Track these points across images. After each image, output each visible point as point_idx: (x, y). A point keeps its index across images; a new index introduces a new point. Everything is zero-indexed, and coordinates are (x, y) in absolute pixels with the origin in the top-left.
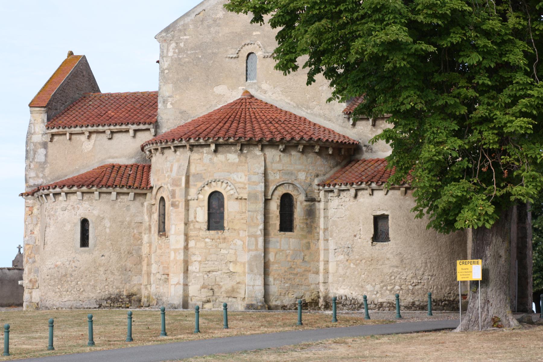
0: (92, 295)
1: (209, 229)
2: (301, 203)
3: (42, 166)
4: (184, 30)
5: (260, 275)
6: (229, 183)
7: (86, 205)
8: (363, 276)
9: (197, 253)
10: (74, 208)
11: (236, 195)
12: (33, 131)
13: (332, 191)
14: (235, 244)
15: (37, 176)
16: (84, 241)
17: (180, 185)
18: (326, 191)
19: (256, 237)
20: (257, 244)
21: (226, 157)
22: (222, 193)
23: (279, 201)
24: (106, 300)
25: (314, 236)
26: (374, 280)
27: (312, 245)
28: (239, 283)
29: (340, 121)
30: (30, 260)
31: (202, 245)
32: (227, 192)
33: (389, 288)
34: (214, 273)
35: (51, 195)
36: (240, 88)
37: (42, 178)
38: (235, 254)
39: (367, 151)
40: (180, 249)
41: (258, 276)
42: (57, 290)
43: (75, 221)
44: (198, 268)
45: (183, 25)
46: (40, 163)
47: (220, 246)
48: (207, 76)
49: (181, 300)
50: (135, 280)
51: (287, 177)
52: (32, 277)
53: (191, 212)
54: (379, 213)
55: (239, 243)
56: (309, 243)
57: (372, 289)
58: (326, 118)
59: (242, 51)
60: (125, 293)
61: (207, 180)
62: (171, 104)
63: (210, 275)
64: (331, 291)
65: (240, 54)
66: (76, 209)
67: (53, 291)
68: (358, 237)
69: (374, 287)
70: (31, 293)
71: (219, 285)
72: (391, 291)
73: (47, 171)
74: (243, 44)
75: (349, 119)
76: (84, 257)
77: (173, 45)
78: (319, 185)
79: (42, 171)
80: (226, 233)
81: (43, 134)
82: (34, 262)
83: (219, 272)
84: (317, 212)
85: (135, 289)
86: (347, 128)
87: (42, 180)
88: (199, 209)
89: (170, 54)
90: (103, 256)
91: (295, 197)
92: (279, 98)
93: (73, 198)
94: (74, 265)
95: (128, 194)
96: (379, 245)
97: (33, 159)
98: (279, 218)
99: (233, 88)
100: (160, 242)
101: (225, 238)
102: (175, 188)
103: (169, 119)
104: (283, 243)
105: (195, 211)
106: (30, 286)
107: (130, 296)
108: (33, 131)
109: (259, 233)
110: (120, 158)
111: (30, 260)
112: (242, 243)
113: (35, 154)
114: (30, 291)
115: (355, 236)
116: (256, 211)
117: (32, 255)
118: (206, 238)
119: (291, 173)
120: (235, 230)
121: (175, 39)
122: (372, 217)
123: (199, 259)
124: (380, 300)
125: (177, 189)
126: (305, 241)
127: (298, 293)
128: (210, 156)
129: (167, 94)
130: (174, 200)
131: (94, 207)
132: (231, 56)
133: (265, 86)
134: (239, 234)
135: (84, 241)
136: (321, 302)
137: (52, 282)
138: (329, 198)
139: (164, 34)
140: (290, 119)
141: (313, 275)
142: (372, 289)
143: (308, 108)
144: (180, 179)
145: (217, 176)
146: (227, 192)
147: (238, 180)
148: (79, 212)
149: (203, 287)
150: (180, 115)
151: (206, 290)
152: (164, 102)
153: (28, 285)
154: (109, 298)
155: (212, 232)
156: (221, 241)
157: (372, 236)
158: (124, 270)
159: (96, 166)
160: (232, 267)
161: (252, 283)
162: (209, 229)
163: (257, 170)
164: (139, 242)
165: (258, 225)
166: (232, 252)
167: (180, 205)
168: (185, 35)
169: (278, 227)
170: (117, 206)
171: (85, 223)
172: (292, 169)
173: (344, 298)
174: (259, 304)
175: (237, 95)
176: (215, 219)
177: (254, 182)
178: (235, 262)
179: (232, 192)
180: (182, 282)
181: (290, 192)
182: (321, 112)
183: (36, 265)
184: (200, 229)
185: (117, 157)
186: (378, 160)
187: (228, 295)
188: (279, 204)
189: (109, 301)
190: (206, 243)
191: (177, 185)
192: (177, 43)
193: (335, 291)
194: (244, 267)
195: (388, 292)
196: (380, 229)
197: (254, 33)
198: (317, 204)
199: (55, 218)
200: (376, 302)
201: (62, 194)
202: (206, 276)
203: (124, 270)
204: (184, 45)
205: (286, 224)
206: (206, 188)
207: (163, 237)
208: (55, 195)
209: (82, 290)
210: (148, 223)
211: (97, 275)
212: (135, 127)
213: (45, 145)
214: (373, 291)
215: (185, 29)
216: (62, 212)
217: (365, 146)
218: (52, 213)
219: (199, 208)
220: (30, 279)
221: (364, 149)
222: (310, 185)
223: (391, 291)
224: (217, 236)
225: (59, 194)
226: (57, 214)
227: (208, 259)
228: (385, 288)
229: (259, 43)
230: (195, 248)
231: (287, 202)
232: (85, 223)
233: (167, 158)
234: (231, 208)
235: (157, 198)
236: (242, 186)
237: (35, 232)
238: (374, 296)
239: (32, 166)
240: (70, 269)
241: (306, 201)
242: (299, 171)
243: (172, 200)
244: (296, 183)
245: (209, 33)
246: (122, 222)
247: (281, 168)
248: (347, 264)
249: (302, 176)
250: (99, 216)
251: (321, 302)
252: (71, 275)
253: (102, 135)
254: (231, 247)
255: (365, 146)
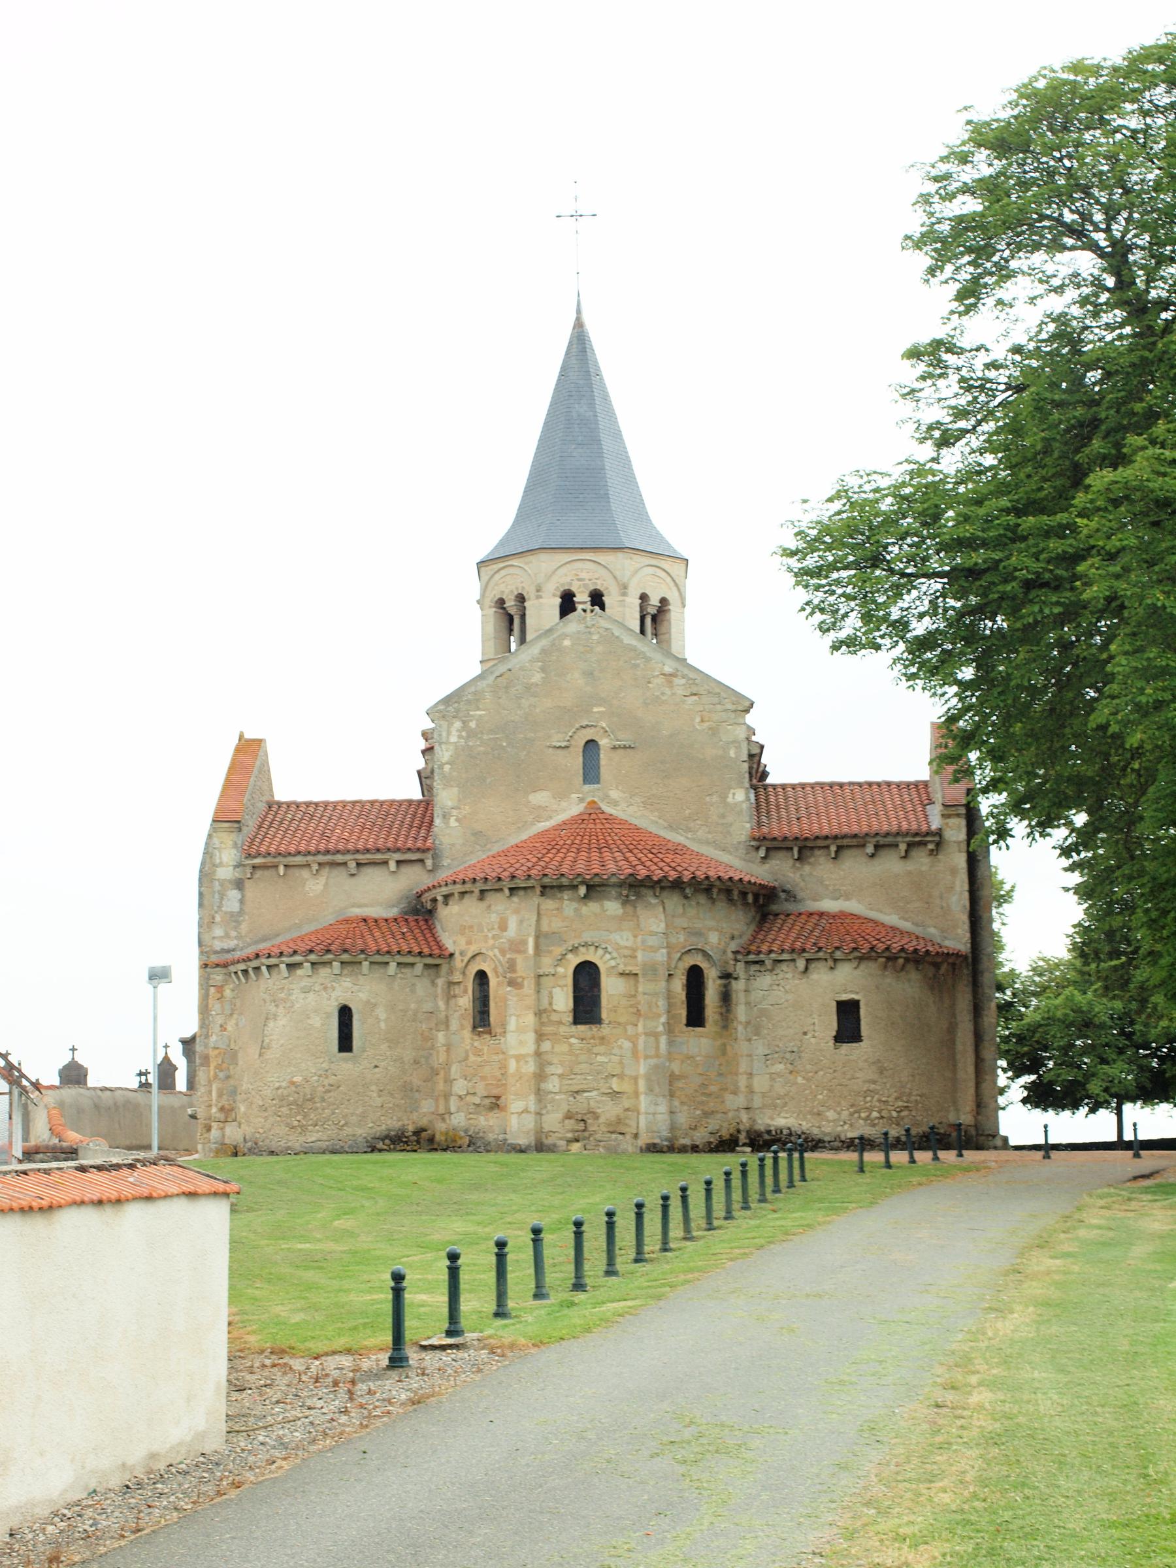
0: (359, 1131)
1: (577, 1021)
2: (714, 981)
3: (234, 919)
4: (476, 701)
5: (664, 1096)
6: (610, 949)
7: (347, 982)
8: (820, 1097)
9: (555, 1061)
10: (325, 988)
11: (621, 968)
12: (218, 861)
13: (761, 962)
14: (621, 1047)
15: (227, 936)
16: (345, 1043)
17: (525, 951)
18: (747, 962)
19: (656, 1035)
20: (657, 1048)
21: (602, 906)
22: (595, 965)
23: (684, 978)
24: (383, 1140)
25: (731, 1035)
26: (839, 1103)
27: (728, 1047)
28: (627, 1110)
29: (742, 851)
30: (221, 1075)
31: (564, 1048)
32: (605, 963)
33: (863, 1115)
34: (586, 1094)
35: (264, 968)
36: (573, 796)
37: (236, 938)
38: (621, 1063)
39: (786, 900)
40: (528, 1055)
41: (661, 1099)
42: (296, 1123)
43: (329, 1009)
44: (558, 1086)
45: (475, 693)
46: (232, 914)
47: (595, 1050)
48: (518, 776)
49: (533, 1138)
50: (427, 1106)
51: (694, 939)
52: (224, 1102)
53: (545, 993)
54: (845, 997)
55: (627, 1045)
56: (724, 1045)
57: (836, 1116)
58: (715, 844)
59: (575, 737)
60: (411, 1128)
61: (571, 943)
62: (457, 820)
63: (578, 1097)
64: (760, 1121)
65: (573, 742)
66: (330, 990)
67: (287, 1125)
68: (809, 1035)
69: (839, 1114)
70: (222, 1129)
71: (594, 1113)
72: (866, 1119)
73: (244, 927)
74: (577, 726)
75: (757, 848)
76: (345, 1065)
77: (458, 724)
78: (736, 953)
79: (235, 928)
80: (605, 1030)
81: (236, 867)
82: (228, 1077)
83: (594, 1093)
84: (734, 996)
85: (423, 1122)
86: (753, 862)
87: (236, 942)
88: (557, 991)
89: (453, 739)
90: (376, 1067)
91: (705, 972)
92: (639, 813)
93: (324, 972)
94: (326, 1082)
95: (413, 965)
96: (845, 1047)
97: (219, 907)
98: (685, 1006)
99: (561, 796)
100: (476, 1044)
101: (603, 1038)
102: (514, 956)
103: (453, 845)
104: (699, 1042)
105: (551, 993)
106: (221, 1116)
107: (418, 1132)
108: (218, 861)
109: (661, 1028)
110: (372, 906)
111: (221, 1075)
112: (630, 1045)
113: (222, 899)
114: (221, 1125)
115: (805, 1033)
116: (656, 994)
117: (225, 1065)
118: (572, 1037)
119: (698, 934)
120: (619, 1024)
121: (461, 714)
122: (835, 1004)
123: (560, 1071)
124: (850, 1135)
125: (519, 959)
126: (719, 1042)
127: (713, 1124)
128: (575, 905)
129: (450, 804)
130: (514, 975)
131: (361, 990)
132: (558, 744)
133: (614, 794)
134: (626, 1030)
135: (345, 1043)
136: (743, 1138)
137: (285, 1110)
138: (751, 973)
139: (442, 707)
140: (659, 848)
141: (731, 1096)
142: (836, 1116)
143: (688, 830)
144: (525, 942)
145: (587, 937)
146: (605, 963)
147: (623, 943)
148: (334, 995)
149: (569, 1116)
150: (473, 838)
151: (572, 1121)
152: (444, 817)
153: (218, 1115)
154: (387, 1137)
155: (581, 1028)
156: (597, 1041)
157: (834, 1033)
158: (408, 1090)
159: (331, 919)
160: (615, 1085)
161: (651, 1110)
162: (577, 1021)
163: (654, 928)
164: (429, 1044)
165: (659, 1016)
166: (615, 1059)
167: (526, 983)
168: (478, 709)
169: (684, 1021)
170: (396, 986)
171: (345, 1013)
172: (700, 926)
173: (785, 1132)
174: (666, 1143)
175: (572, 808)
176: (586, 1007)
177: (651, 947)
178: (621, 1076)
179: (613, 963)
180: (532, 1107)
181: (699, 963)
182: (710, 836)
183: (232, 1082)
184: (560, 1023)
185: (366, 905)
186: (821, 914)
187: (611, 1129)
188: (685, 982)
189: (387, 1141)
190: (571, 1045)
191: (519, 952)
192: (464, 722)
193: (769, 1121)
194: (636, 1083)
195: (861, 1122)
196: (848, 1019)
197: (595, 710)
198: (733, 982)
199: (288, 1005)
200: (843, 1138)
201: (334, 963)
202: (571, 1099)
203: (408, 1090)
204: (477, 725)
205: (695, 1018)
206: (570, 956)
207: (486, 1036)
208: (291, 966)
209: (343, 1122)
210: (444, 1014)
211: (367, 1099)
212: (398, 856)
213: (239, 884)
214: (838, 1120)
215: (478, 700)
216: (303, 995)
217: (784, 891)
218: (282, 995)
219: (558, 989)
220: (220, 1105)
221: (783, 895)
222: (725, 952)
223: (866, 1119)
224: (589, 1034)
225: (298, 965)
226: (293, 997)
227: (576, 1070)
228: (856, 1115)
229: (604, 725)
230: (553, 1053)
231: (695, 978)
232: (345, 1013)
233: (489, 906)
234: (611, 988)
235: (467, 973)
236: (627, 952)
237: (229, 1028)
238: (839, 1129)
239: (218, 918)
240: (320, 1089)
241: (720, 978)
242: (710, 929)
243: (508, 975)
244: (707, 948)
245: (519, 707)
246: (405, 1011)
247: (685, 925)
248: (791, 1077)
249: (714, 938)
250: (368, 1002)
251: (743, 1138)
252: (323, 1100)
253: (341, 869)
254: (614, 1051)
255: (784, 891)
